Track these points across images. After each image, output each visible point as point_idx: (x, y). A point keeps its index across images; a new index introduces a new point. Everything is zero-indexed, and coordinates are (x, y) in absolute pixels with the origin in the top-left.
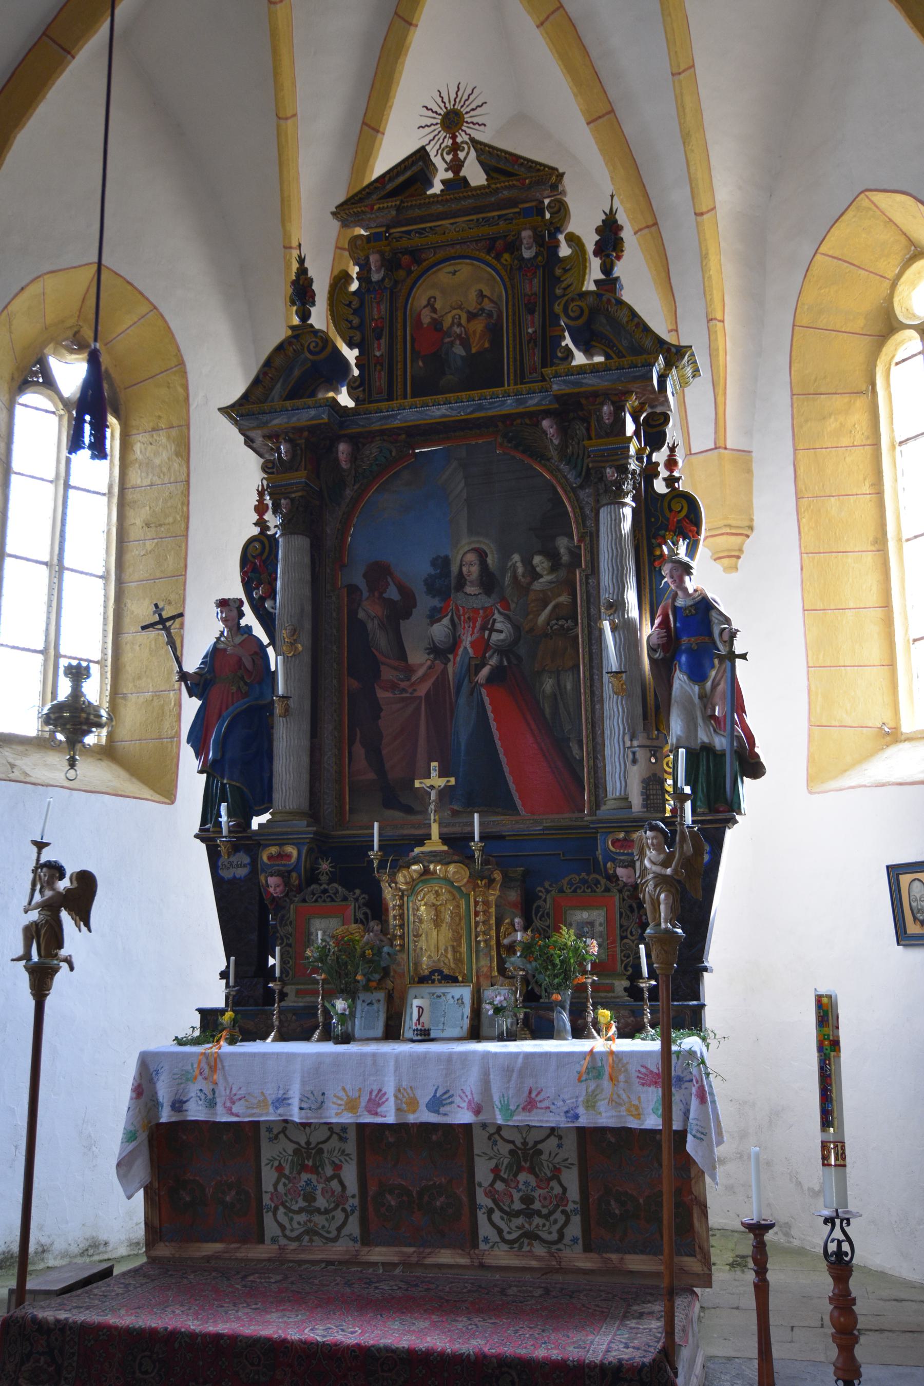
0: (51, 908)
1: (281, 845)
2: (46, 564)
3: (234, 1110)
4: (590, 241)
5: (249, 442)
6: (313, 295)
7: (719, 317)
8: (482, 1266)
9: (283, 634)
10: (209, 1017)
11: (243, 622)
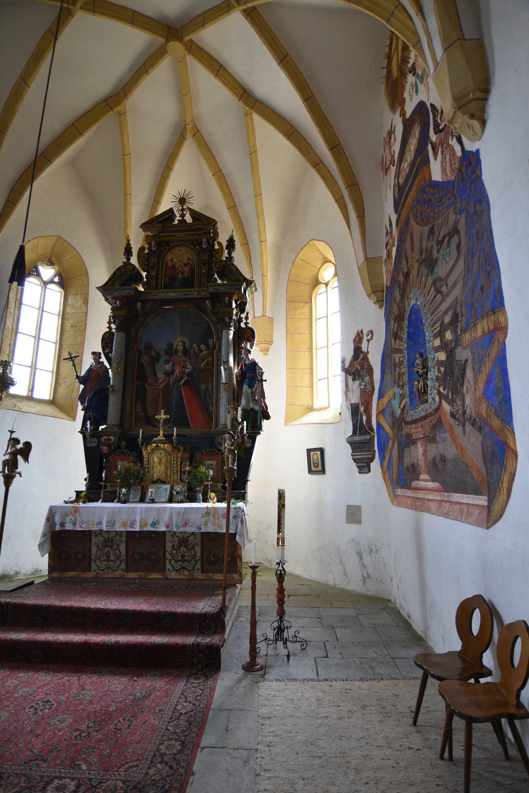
0: (14, 455)
1: (108, 436)
2: (33, 337)
3: (83, 526)
4: (225, 244)
5: (106, 300)
6: (132, 253)
7: (266, 275)
8: (167, 579)
9: (114, 365)
10: (78, 493)
11: (101, 360)
